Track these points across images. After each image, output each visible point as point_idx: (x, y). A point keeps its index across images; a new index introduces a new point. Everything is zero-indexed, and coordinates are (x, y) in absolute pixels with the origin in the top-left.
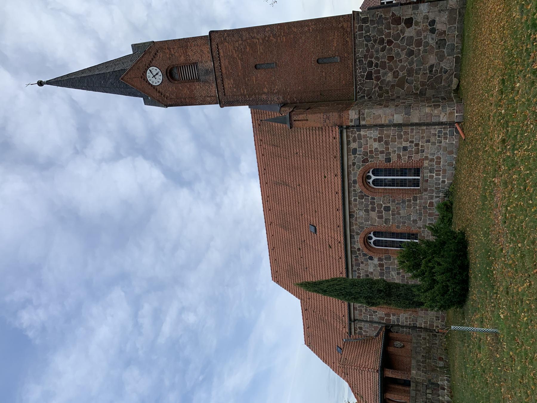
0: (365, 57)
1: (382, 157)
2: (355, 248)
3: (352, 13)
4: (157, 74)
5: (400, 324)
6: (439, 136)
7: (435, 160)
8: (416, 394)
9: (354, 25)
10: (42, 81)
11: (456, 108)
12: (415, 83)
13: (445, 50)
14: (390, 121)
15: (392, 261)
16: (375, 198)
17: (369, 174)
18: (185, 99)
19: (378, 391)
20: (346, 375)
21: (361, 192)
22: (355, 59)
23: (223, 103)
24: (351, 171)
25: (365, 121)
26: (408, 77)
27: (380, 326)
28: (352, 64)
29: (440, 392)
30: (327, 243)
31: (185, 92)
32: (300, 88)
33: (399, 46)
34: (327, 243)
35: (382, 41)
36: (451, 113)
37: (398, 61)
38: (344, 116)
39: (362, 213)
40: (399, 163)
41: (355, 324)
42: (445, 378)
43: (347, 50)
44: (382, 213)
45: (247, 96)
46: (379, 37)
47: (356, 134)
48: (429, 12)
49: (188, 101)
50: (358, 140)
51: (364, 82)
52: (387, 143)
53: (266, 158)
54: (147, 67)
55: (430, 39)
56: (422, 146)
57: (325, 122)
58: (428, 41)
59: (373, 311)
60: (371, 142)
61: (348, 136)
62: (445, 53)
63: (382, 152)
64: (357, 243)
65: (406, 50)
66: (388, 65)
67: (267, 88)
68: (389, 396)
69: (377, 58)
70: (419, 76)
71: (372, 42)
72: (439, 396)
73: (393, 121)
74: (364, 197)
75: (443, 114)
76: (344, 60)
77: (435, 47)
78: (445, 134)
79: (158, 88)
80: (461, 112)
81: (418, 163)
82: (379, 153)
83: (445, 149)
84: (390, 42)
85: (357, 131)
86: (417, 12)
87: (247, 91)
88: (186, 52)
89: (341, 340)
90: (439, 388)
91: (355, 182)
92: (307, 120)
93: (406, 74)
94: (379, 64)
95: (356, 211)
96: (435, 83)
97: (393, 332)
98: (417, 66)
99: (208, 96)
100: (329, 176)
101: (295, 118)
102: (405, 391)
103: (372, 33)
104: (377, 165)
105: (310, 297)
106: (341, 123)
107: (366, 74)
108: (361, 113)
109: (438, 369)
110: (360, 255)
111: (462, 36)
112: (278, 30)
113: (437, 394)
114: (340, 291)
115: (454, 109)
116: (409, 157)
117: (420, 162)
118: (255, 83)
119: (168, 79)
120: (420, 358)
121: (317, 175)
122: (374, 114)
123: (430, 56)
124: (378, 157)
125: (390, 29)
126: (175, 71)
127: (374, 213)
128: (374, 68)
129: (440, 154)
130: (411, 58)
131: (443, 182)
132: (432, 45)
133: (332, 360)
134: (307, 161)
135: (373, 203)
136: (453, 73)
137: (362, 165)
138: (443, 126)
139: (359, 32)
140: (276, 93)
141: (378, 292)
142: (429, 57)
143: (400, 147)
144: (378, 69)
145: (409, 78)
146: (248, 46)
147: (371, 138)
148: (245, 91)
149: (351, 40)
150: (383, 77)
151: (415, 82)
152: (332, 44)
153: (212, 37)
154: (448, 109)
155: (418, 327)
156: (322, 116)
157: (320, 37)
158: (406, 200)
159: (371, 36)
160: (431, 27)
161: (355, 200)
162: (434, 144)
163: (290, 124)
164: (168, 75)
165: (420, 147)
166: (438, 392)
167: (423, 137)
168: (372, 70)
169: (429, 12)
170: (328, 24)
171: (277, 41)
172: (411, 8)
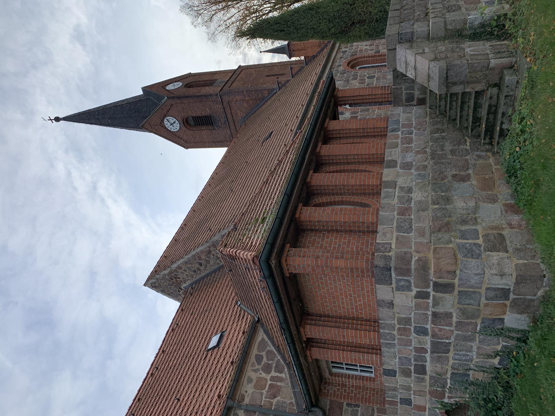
4: (174, 123)
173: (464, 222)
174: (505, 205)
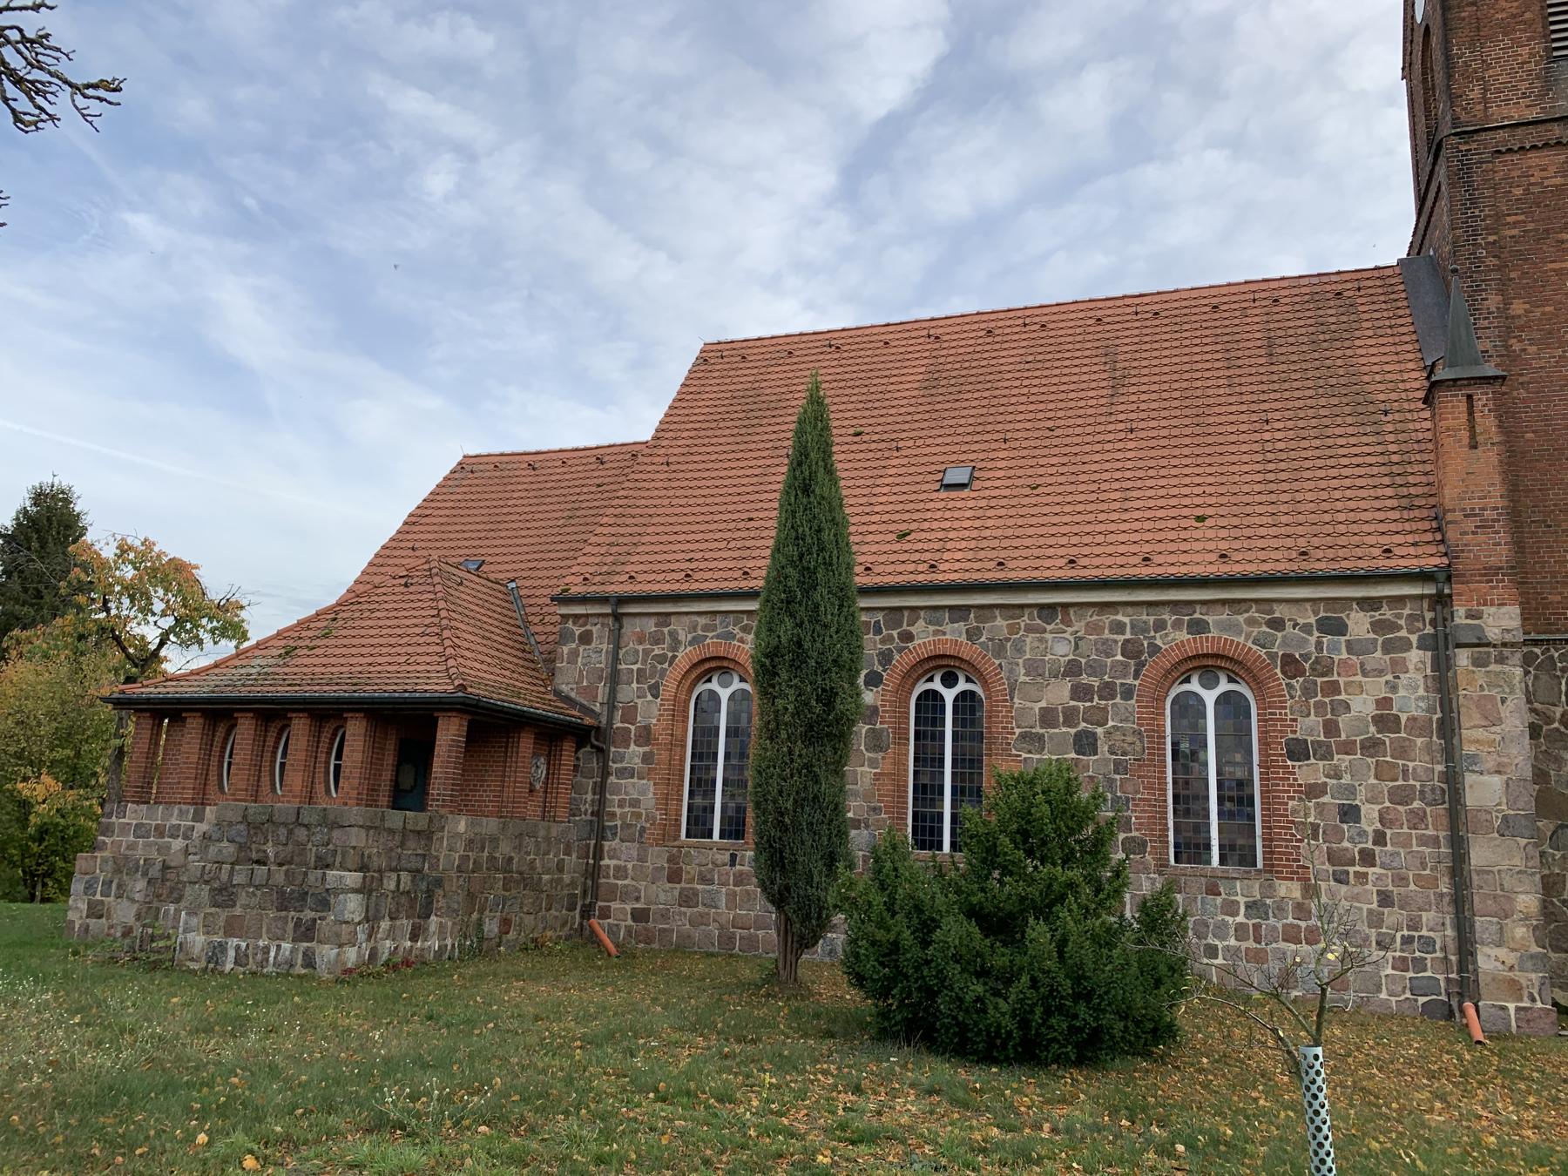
1: (1309, 727)
5: (612, 779)
6: (1407, 941)
7: (1303, 924)
8: (391, 831)
11: (1541, 1009)
12: (1554, 855)
15: (867, 754)
16: (1133, 702)
19: (375, 691)
20: (403, 581)
21: (1155, 650)
24: (1247, 611)
25: (1471, 668)
27: (597, 708)
29: (405, 922)
30: (914, 526)
32: (1529, 436)
34: (914, 526)
36: (1515, 989)
39: (1061, 650)
40: (1289, 792)
41: (601, 619)
42: (449, 942)
45: (1495, 237)
47: (1410, 632)
49: (1463, 14)
50: (1380, 640)
51: (1559, 673)
52: (1371, 747)
57: (1465, 516)
59: (657, 682)
60: (1376, 687)
61: (1400, 600)
63: (1331, 728)
68: (356, 731)
72: (392, 919)
73: (1473, 771)
74: (1132, 662)
75: (1511, 958)
78: (1420, 965)
80: (1523, 1024)
81: (1288, 860)
82: (1329, 716)
85: (1420, 639)
87: (1514, 237)
89: (511, 575)
90: (417, 920)
91: (1198, 627)
92: (1474, 446)
97: (576, 752)
99: (1486, 90)
101: (1483, 398)
102: (373, 790)
104: (1276, 708)
105: (673, 468)
108: (1506, 652)
109: (475, 916)
113: (398, 910)
114: (816, 548)
115: (1534, 1000)
116: (1315, 827)
117: (1292, 866)
120: (505, 848)
122: (1503, 701)
133: (423, 544)
135: (1108, 691)
138: (1453, 958)
140: (1507, 347)
147: (1394, 688)
148: (1515, 232)
151: (1558, 855)
154: (1533, 976)
155: (602, 846)
156: (1492, 502)
161: (1119, 628)
163: (1455, 380)
165: (1358, 868)
166: (403, 914)
167: (1401, 880)
173: (119, 886)
174: (131, 928)
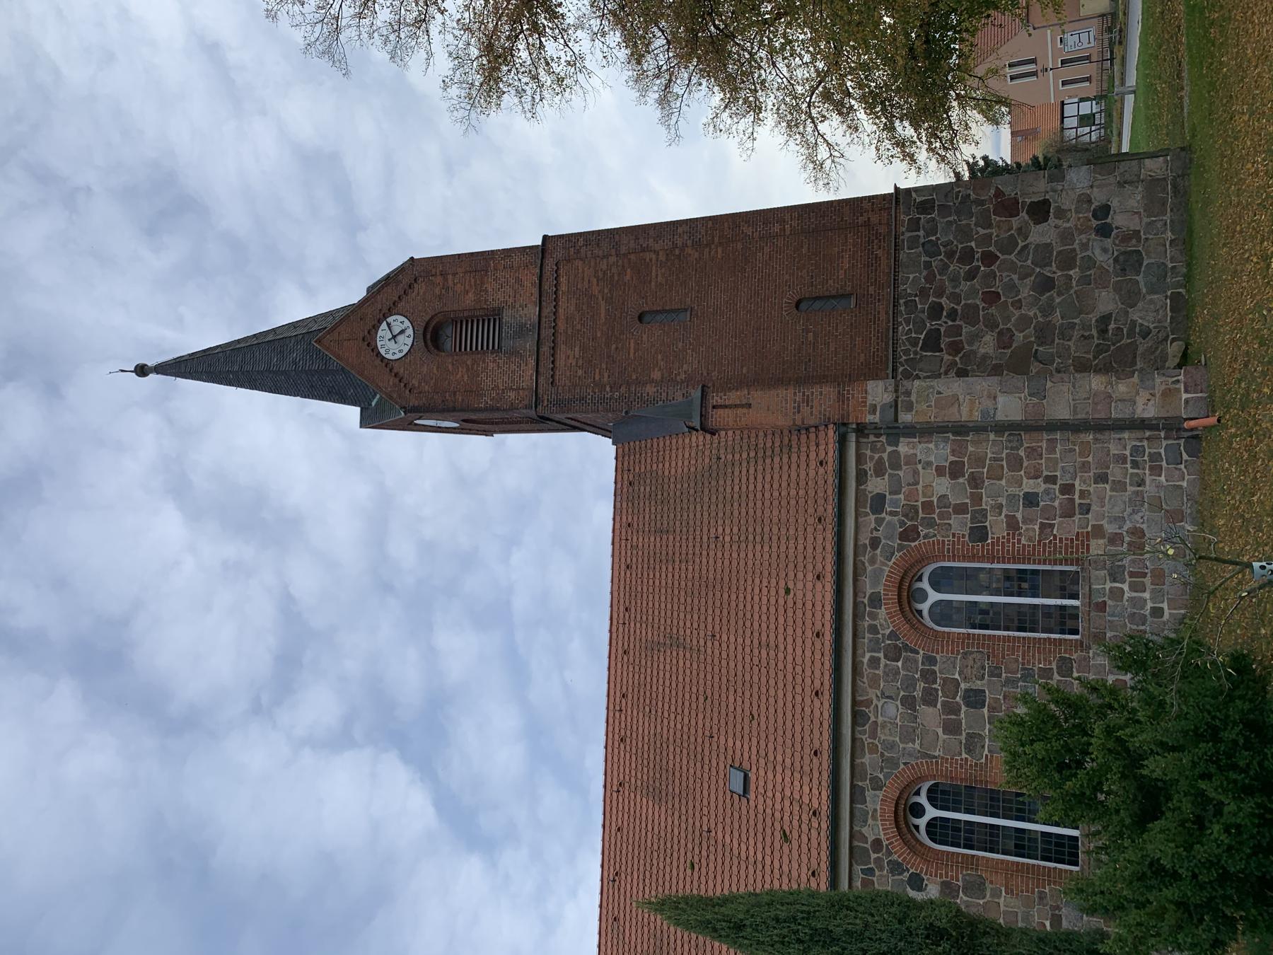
0: (923, 293)
1: (960, 525)
2: (865, 839)
3: (892, 191)
4: (402, 332)
6: (1135, 464)
9: (896, 217)
10: (146, 365)
11: (1185, 376)
13: (1140, 278)
14: (985, 413)
17: (919, 585)
18: (455, 393)
21: (893, 635)
22: (894, 298)
23: (546, 403)
25: (914, 413)
26: (1038, 345)
28: (887, 313)
31: (458, 376)
33: (1013, 268)
35: (968, 256)
36: (1168, 393)
37: (1012, 304)
38: (853, 397)
39: (893, 710)
40: (1014, 543)
43: (876, 280)
44: (956, 711)
46: (960, 246)
47: (884, 451)
48: (1092, 187)
50: (890, 471)
52: (975, 481)
53: (634, 576)
54: (384, 315)
55: (1097, 252)
56: (1082, 492)
58: (1091, 255)
60: (926, 476)
62: (1142, 284)
63: (960, 509)
64: (874, 818)
65: (1033, 278)
66: (983, 315)
67: (660, 369)
69: (955, 298)
70: (1069, 343)
71: (942, 257)
73: (994, 414)
74: (904, 654)
76: (868, 302)
77: (1111, 270)
79: (396, 365)
82: (951, 510)
83: (1156, 505)
84: (989, 258)
85: (889, 445)
86: (1060, 188)
88: (482, 283)
91: (876, 601)
92: (749, 406)
93: (1033, 339)
94: (959, 312)
95: (875, 702)
96: (1115, 362)
98: (1062, 318)
100: (800, 585)
101: (715, 399)
103: (942, 237)
106: (843, 415)
107: (922, 337)
108: (901, 389)
110: (881, 869)
111: (1186, 241)
112: (707, 231)
115: (1178, 381)
116: (1042, 526)
118: (632, 355)
119: (426, 346)
121: (765, 591)
122: (939, 393)
123: (1100, 293)
124: (950, 525)
125: (990, 226)
126: (449, 331)
127: (931, 709)
128: (946, 323)
129: (1143, 519)
130: (1048, 298)
131: (1157, 612)
132: (1103, 264)
134: (743, 555)
135: (929, 676)
136: (1168, 336)
137: (901, 548)
139: (908, 234)
140: (682, 382)
141: (927, 937)
142: (1097, 295)
143: (1014, 496)
144: (957, 323)
145: (1041, 349)
146: (629, 270)
147: (928, 464)
148: (606, 375)
149: (889, 253)
150: (970, 343)
151: (1058, 360)
152: (838, 264)
153: (549, 246)
157: (809, 249)
158: (1036, 669)
159: (939, 242)
160: (1100, 222)
161: (874, 662)
162: (1119, 486)
163: (701, 416)
164: (428, 336)
165: (1076, 496)
167: (1085, 467)
168: (941, 325)
169: (1092, 187)
170: (831, 217)
171: (700, 258)
172: (1044, 177)
